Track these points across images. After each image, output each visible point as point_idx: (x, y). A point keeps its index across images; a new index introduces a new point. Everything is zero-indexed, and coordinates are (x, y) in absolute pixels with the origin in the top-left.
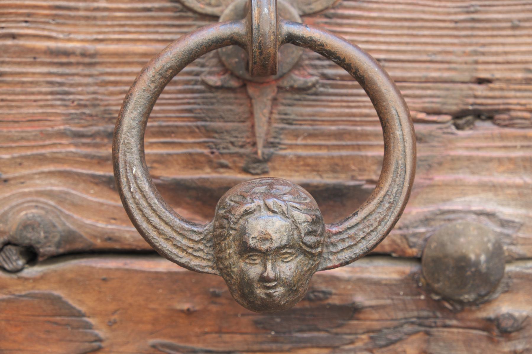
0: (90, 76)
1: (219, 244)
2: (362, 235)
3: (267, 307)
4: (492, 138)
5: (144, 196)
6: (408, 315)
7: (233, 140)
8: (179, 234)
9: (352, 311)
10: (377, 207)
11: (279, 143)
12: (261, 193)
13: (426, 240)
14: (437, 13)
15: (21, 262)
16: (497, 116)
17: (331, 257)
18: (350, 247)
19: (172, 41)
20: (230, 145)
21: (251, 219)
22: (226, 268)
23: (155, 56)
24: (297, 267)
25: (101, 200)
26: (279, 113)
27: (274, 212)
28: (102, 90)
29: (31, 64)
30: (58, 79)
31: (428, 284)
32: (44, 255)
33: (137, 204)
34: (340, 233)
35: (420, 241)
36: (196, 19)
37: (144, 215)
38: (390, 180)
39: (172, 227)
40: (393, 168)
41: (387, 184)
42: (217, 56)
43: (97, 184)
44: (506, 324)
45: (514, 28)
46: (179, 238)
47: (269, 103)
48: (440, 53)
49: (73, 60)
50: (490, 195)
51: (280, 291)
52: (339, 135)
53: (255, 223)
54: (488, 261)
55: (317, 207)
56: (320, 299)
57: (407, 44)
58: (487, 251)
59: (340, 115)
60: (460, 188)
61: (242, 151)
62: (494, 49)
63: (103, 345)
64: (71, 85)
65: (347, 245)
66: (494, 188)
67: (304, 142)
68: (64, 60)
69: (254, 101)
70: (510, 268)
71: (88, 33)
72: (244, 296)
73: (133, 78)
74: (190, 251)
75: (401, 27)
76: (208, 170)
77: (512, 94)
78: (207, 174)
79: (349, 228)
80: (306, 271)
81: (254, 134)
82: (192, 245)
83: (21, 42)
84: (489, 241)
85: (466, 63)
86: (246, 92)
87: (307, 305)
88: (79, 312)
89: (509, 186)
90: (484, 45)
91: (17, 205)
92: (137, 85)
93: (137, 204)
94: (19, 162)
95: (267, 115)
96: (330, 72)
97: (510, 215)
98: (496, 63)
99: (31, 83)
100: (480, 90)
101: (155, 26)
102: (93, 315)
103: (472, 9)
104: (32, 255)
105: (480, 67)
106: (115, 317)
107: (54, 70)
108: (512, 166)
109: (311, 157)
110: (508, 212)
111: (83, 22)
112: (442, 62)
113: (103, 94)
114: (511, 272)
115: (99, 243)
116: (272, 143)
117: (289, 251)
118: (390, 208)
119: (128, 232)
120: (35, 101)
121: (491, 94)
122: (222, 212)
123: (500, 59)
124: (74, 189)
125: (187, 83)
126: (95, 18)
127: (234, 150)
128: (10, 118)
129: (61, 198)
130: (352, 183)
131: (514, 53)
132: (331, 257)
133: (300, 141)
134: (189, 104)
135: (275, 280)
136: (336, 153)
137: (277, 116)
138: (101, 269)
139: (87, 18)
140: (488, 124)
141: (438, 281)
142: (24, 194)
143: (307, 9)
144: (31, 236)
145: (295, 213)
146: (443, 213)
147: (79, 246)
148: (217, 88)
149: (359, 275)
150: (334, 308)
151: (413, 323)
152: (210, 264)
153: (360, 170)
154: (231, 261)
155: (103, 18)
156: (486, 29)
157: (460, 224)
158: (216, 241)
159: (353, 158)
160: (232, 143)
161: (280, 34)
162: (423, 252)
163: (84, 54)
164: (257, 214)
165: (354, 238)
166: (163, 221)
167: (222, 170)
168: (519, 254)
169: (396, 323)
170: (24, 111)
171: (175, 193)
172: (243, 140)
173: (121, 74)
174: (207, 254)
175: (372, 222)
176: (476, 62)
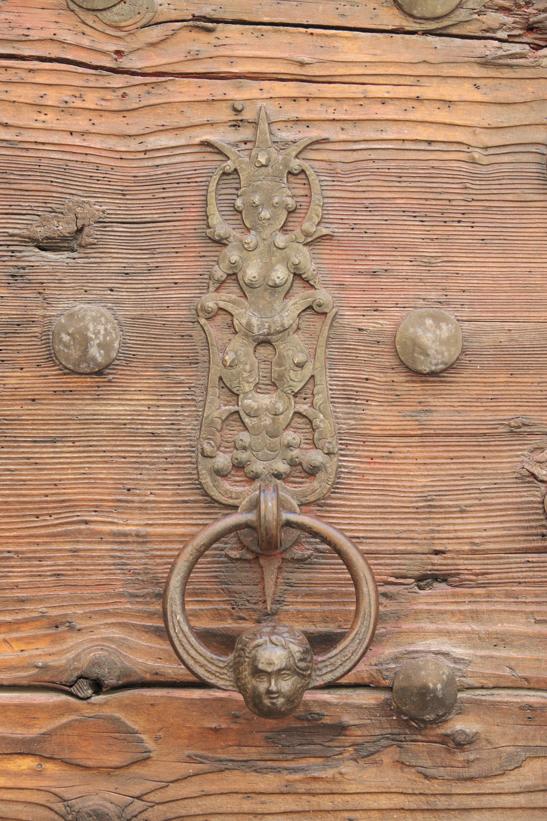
0: (143, 551)
1: (238, 668)
2: (339, 662)
3: (272, 713)
4: (446, 595)
5: (185, 635)
6: (383, 732)
7: (249, 598)
8: (210, 662)
9: (341, 729)
10: (351, 643)
11: (283, 601)
12: (267, 632)
13: (396, 674)
14: (403, 502)
15: (90, 692)
16: (450, 579)
17: (318, 679)
18: (332, 671)
19: (206, 525)
20: (246, 602)
21: (260, 650)
22: (243, 685)
23: (193, 536)
24: (293, 684)
25: (150, 645)
26: (283, 579)
27: (276, 645)
28: (151, 562)
29: (99, 543)
30: (119, 554)
31: (398, 707)
32: (108, 685)
33: (180, 641)
34: (324, 661)
35: (392, 675)
36: (221, 509)
37: (185, 649)
38: (359, 623)
39: (204, 657)
40: (362, 614)
41: (358, 626)
42: (237, 536)
43: (147, 632)
44: (460, 738)
45: (462, 511)
46: (209, 665)
47: (276, 571)
48: (405, 531)
49: (130, 539)
50: (446, 639)
51: (281, 700)
52: (329, 594)
53: (262, 652)
54: (442, 689)
55: (307, 642)
56: (316, 720)
57: (380, 525)
58: (442, 681)
59: (329, 579)
60: (422, 634)
61: (255, 607)
62: (447, 528)
63: (151, 755)
64: (128, 558)
65: (329, 669)
66: (448, 633)
67: (302, 600)
68: (123, 540)
69: (264, 569)
70: (460, 695)
71: (141, 520)
72: (255, 705)
73: (176, 553)
74: (217, 674)
75: (375, 513)
76: (230, 621)
77: (461, 561)
78: (229, 624)
79: (331, 658)
80: (300, 688)
81: (264, 595)
82: (218, 670)
83: (92, 527)
84: (444, 673)
85: (425, 539)
86: (259, 562)
87: (306, 724)
88: (133, 729)
89: (460, 632)
90: (439, 525)
91: (88, 648)
92: (180, 557)
93: (180, 641)
94: (89, 616)
95: (274, 580)
96: (319, 546)
97: (461, 654)
98: (448, 538)
99: (99, 556)
100: (436, 559)
101: (191, 514)
102: (144, 732)
103: (429, 498)
104: (98, 686)
105: (436, 541)
106: (161, 734)
107: (116, 547)
108: (462, 617)
109: (307, 611)
110: (459, 652)
111: (137, 511)
112: (407, 539)
113: (152, 565)
114: (463, 698)
115: (148, 677)
116: (278, 601)
117: (287, 672)
118: (359, 643)
119: (170, 668)
120: (101, 570)
121: (444, 562)
122: (240, 646)
123: (451, 535)
124: (129, 636)
125: (214, 556)
126: (146, 508)
127: (249, 606)
128: (83, 583)
129: (121, 642)
130: (339, 631)
131: (462, 531)
132: (318, 679)
133: (299, 600)
134: (216, 572)
135: (277, 692)
136: (326, 608)
137: (282, 581)
138: (149, 696)
139: (140, 508)
140: (443, 585)
141: (406, 705)
142: (93, 640)
143: (304, 500)
144: (96, 672)
145: (291, 646)
146: (409, 653)
147: (133, 679)
148: (237, 560)
149: (345, 701)
150: (326, 726)
151: (388, 738)
152: (232, 684)
153: (345, 621)
154: (246, 680)
155: (153, 508)
156: (441, 513)
157: (421, 661)
158: (236, 667)
159: (339, 612)
160: (248, 601)
161: (281, 520)
162: (393, 683)
163: (138, 536)
164: (264, 646)
165: (334, 665)
166: (199, 653)
167: (241, 621)
168: (469, 684)
169: (374, 738)
170: (93, 577)
171: (207, 637)
172: (257, 598)
173: (165, 550)
174: (230, 676)
175: (347, 653)
176: (434, 539)
